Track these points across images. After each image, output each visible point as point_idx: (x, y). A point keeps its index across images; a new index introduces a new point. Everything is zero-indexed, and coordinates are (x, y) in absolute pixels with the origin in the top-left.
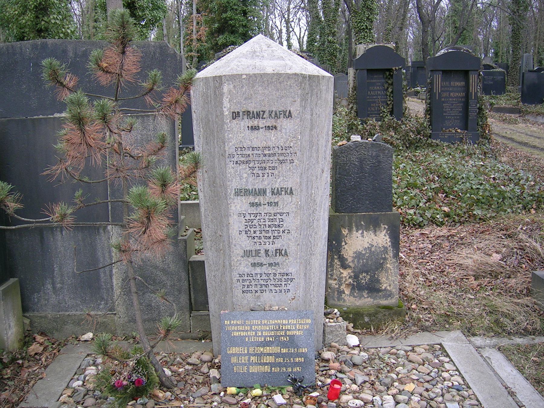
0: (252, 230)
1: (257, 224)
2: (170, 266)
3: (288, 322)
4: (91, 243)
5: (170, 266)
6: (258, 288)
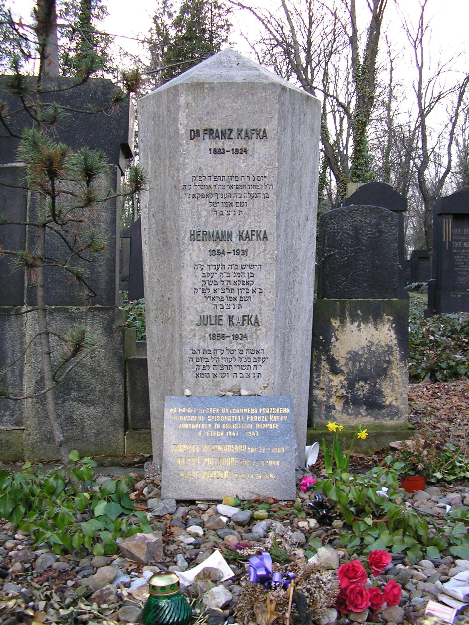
0: (212, 288)
1: (218, 280)
2: (101, 364)
3: (258, 411)
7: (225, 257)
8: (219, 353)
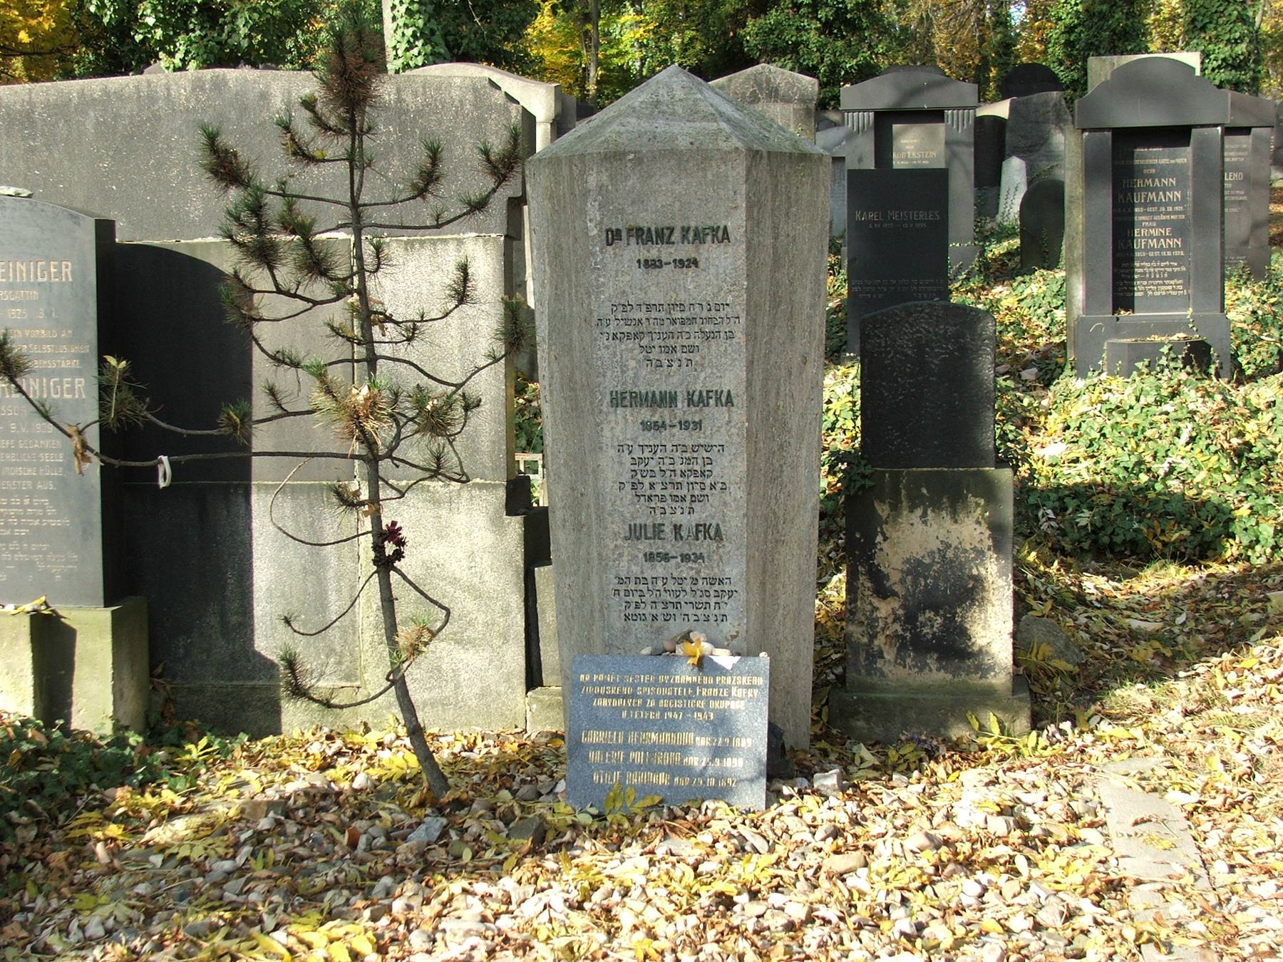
2: (486, 578)
4: (312, 523)
5: (486, 578)
6: (659, 610)
7: (665, 433)
8: (660, 583)
